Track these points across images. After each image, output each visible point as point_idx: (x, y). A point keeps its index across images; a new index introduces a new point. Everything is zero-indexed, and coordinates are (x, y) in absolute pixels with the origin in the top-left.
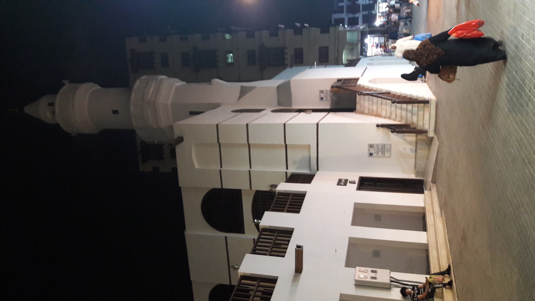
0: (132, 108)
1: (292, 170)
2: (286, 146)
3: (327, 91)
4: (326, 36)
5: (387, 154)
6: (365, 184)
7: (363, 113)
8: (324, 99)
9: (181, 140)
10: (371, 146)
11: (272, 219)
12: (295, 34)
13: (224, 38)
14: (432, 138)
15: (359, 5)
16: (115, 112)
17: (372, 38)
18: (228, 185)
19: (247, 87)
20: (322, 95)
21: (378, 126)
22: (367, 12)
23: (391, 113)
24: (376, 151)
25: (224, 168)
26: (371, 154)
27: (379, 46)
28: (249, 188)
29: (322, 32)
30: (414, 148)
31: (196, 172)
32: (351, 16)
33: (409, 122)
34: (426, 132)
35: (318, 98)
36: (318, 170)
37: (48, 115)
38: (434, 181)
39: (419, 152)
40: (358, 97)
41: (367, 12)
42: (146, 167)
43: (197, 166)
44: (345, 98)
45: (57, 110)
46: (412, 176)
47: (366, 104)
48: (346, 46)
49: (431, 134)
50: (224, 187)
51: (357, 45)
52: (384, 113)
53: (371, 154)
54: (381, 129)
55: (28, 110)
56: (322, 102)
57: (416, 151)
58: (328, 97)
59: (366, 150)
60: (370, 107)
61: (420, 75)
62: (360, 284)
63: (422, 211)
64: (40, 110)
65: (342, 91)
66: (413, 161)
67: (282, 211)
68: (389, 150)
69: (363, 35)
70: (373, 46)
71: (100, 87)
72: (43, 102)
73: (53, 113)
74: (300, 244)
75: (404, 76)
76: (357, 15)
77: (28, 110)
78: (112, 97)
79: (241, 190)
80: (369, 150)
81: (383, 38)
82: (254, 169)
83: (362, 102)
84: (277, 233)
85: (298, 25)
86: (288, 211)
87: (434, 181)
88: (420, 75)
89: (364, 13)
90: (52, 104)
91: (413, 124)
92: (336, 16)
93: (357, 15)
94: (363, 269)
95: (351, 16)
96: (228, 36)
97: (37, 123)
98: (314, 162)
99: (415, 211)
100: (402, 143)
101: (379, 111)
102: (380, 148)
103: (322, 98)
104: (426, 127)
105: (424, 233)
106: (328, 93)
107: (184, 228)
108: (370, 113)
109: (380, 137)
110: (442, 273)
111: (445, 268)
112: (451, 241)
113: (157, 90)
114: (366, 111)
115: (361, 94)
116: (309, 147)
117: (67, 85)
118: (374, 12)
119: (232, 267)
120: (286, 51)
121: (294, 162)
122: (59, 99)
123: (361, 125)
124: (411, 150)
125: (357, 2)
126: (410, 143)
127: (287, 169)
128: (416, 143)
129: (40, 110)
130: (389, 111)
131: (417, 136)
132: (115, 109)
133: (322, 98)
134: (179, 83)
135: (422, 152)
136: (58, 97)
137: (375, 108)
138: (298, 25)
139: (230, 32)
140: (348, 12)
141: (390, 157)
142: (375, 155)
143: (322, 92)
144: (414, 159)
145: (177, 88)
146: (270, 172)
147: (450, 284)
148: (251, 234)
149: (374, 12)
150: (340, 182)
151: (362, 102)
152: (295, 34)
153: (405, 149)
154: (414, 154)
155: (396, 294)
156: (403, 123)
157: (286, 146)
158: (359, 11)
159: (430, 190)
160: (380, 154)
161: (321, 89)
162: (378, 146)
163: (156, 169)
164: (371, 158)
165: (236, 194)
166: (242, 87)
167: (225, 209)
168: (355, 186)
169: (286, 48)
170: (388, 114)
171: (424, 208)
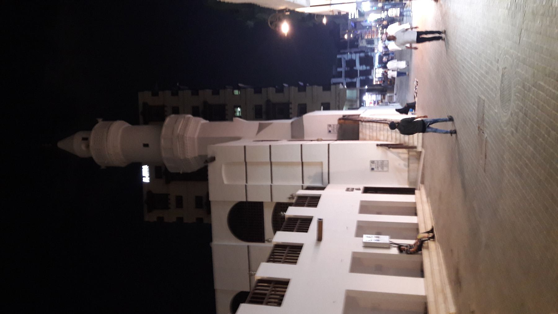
0: (162, 141)
1: (307, 184)
2: (302, 163)
3: (334, 125)
4: (327, 93)
5: (385, 169)
6: (367, 190)
7: (365, 140)
8: (332, 131)
9: (213, 159)
10: (373, 162)
11: (284, 237)
12: (299, 91)
13: (233, 93)
14: (421, 152)
15: (357, 71)
16: (146, 145)
17: (370, 96)
18: (252, 198)
19: (265, 123)
20: (330, 129)
21: (377, 145)
22: (364, 78)
23: (388, 137)
24: (377, 166)
25: (250, 183)
26: (373, 169)
27: (376, 103)
28: (270, 200)
29: (324, 89)
30: (407, 164)
31: (226, 188)
32: (349, 80)
33: (402, 142)
34: (415, 147)
35: (327, 131)
36: (329, 183)
37: (83, 147)
38: (423, 182)
39: (411, 165)
40: (360, 123)
41: (364, 78)
42: (151, 217)
43: (226, 182)
44: (349, 130)
45: (91, 144)
46: (407, 186)
47: (368, 132)
48: (346, 103)
49: (419, 149)
50: (250, 200)
51: (356, 101)
52: (382, 138)
53: (373, 169)
54: (380, 148)
55: (61, 145)
56: (330, 134)
57: (408, 166)
58: (335, 130)
59: (368, 166)
60: (371, 134)
61: (411, 109)
62: (367, 245)
63: (413, 206)
64: (75, 145)
65: (347, 122)
66: (406, 175)
67: (293, 231)
68: (387, 166)
69: (362, 93)
70: (371, 103)
71: (130, 125)
72: (78, 137)
73: (88, 146)
74: (321, 218)
75: (398, 110)
76: (355, 80)
77: (61, 145)
78: (143, 133)
79: (262, 202)
80: (371, 166)
81: (380, 96)
82: (275, 183)
83: (364, 131)
84: (288, 249)
85: (301, 84)
86: (299, 231)
87: (423, 182)
88: (411, 109)
89: (362, 78)
90: (86, 139)
91: (405, 143)
92: (334, 80)
93: (355, 80)
94: (369, 236)
95: (349, 80)
96: (236, 92)
97: (70, 157)
98: (326, 176)
99: (408, 206)
100: (397, 159)
101: (379, 137)
102: (380, 163)
103: (330, 131)
104: (416, 144)
105: (421, 280)
106: (335, 127)
107: (210, 239)
108: (371, 139)
109: (379, 154)
110: (428, 232)
111: (429, 228)
112: (434, 212)
113: (186, 126)
114: (368, 138)
115: (362, 121)
116: (321, 163)
117: (101, 123)
118: (370, 77)
119: (251, 270)
120: (291, 106)
121: (309, 177)
122: (93, 135)
123: (365, 149)
124: (405, 165)
125: (355, 68)
126: (404, 159)
127: (303, 183)
128: (409, 159)
129: (75, 145)
130: (386, 135)
131: (409, 152)
132: (146, 143)
133: (330, 131)
134: (203, 121)
135: (413, 166)
136: (93, 132)
137: (375, 134)
138: (301, 84)
139: (239, 88)
140: (346, 76)
141: (387, 171)
142: (375, 169)
143: (330, 126)
144: (407, 173)
145: (203, 124)
146: (288, 184)
147: (433, 237)
148: (267, 247)
149: (370, 77)
150: (348, 190)
151: (364, 130)
152: (299, 91)
153: (399, 164)
154: (407, 169)
155: (394, 251)
156: (398, 142)
157: (302, 163)
158: (357, 76)
159: (420, 190)
160: (380, 169)
161: (330, 123)
162: (378, 161)
163: (161, 219)
164: (373, 173)
165: (259, 206)
166: (260, 124)
167: (248, 220)
168: (361, 191)
169: (291, 103)
170: (386, 138)
171: (415, 203)
